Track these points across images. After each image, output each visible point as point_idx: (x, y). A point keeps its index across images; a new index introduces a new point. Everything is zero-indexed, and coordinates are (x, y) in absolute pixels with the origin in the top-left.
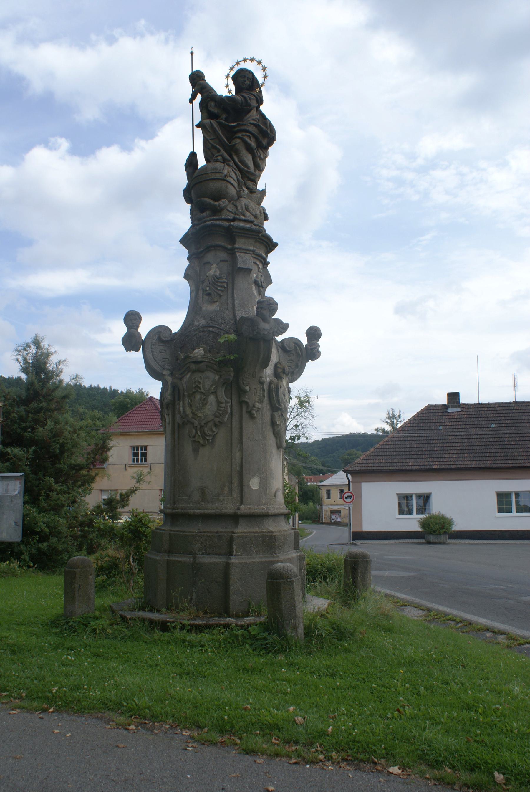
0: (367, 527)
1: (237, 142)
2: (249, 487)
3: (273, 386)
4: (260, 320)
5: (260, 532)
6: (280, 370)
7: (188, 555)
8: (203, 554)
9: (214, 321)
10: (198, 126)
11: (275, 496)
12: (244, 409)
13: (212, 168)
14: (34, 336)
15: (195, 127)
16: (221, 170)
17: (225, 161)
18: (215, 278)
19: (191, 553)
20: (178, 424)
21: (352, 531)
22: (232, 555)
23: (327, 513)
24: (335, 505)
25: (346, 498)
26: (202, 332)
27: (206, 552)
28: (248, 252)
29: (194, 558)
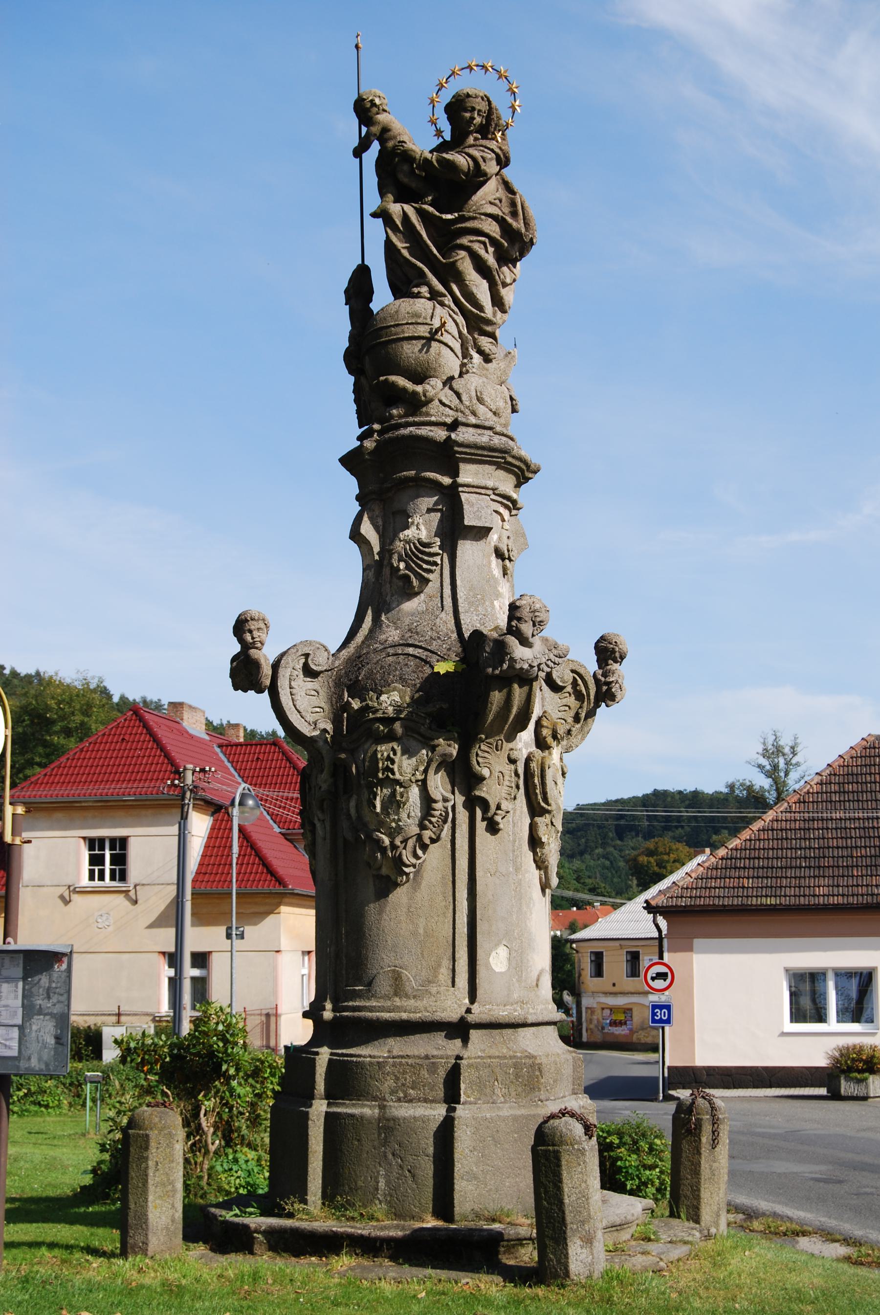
0: (704, 1058)
1: (458, 258)
2: (488, 966)
3: (534, 765)
4: (512, 641)
5: (511, 1057)
6: (545, 732)
7: (368, 1103)
8: (399, 1100)
9: (417, 633)
10: (374, 215)
11: (537, 985)
12: (479, 813)
13: (408, 313)
14: (824, 1054)
15: (367, 218)
16: (429, 317)
17: (434, 296)
18: (418, 545)
19: (375, 1099)
20: (345, 839)
21: (667, 1064)
22: (458, 1102)
23: (595, 1017)
24: (615, 994)
25: (653, 979)
26: (393, 655)
27: (405, 1097)
28: (483, 491)
29: (382, 1107)
